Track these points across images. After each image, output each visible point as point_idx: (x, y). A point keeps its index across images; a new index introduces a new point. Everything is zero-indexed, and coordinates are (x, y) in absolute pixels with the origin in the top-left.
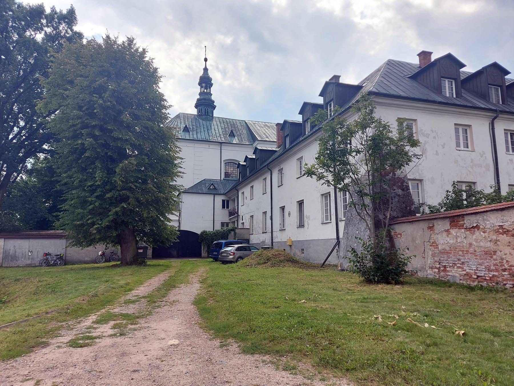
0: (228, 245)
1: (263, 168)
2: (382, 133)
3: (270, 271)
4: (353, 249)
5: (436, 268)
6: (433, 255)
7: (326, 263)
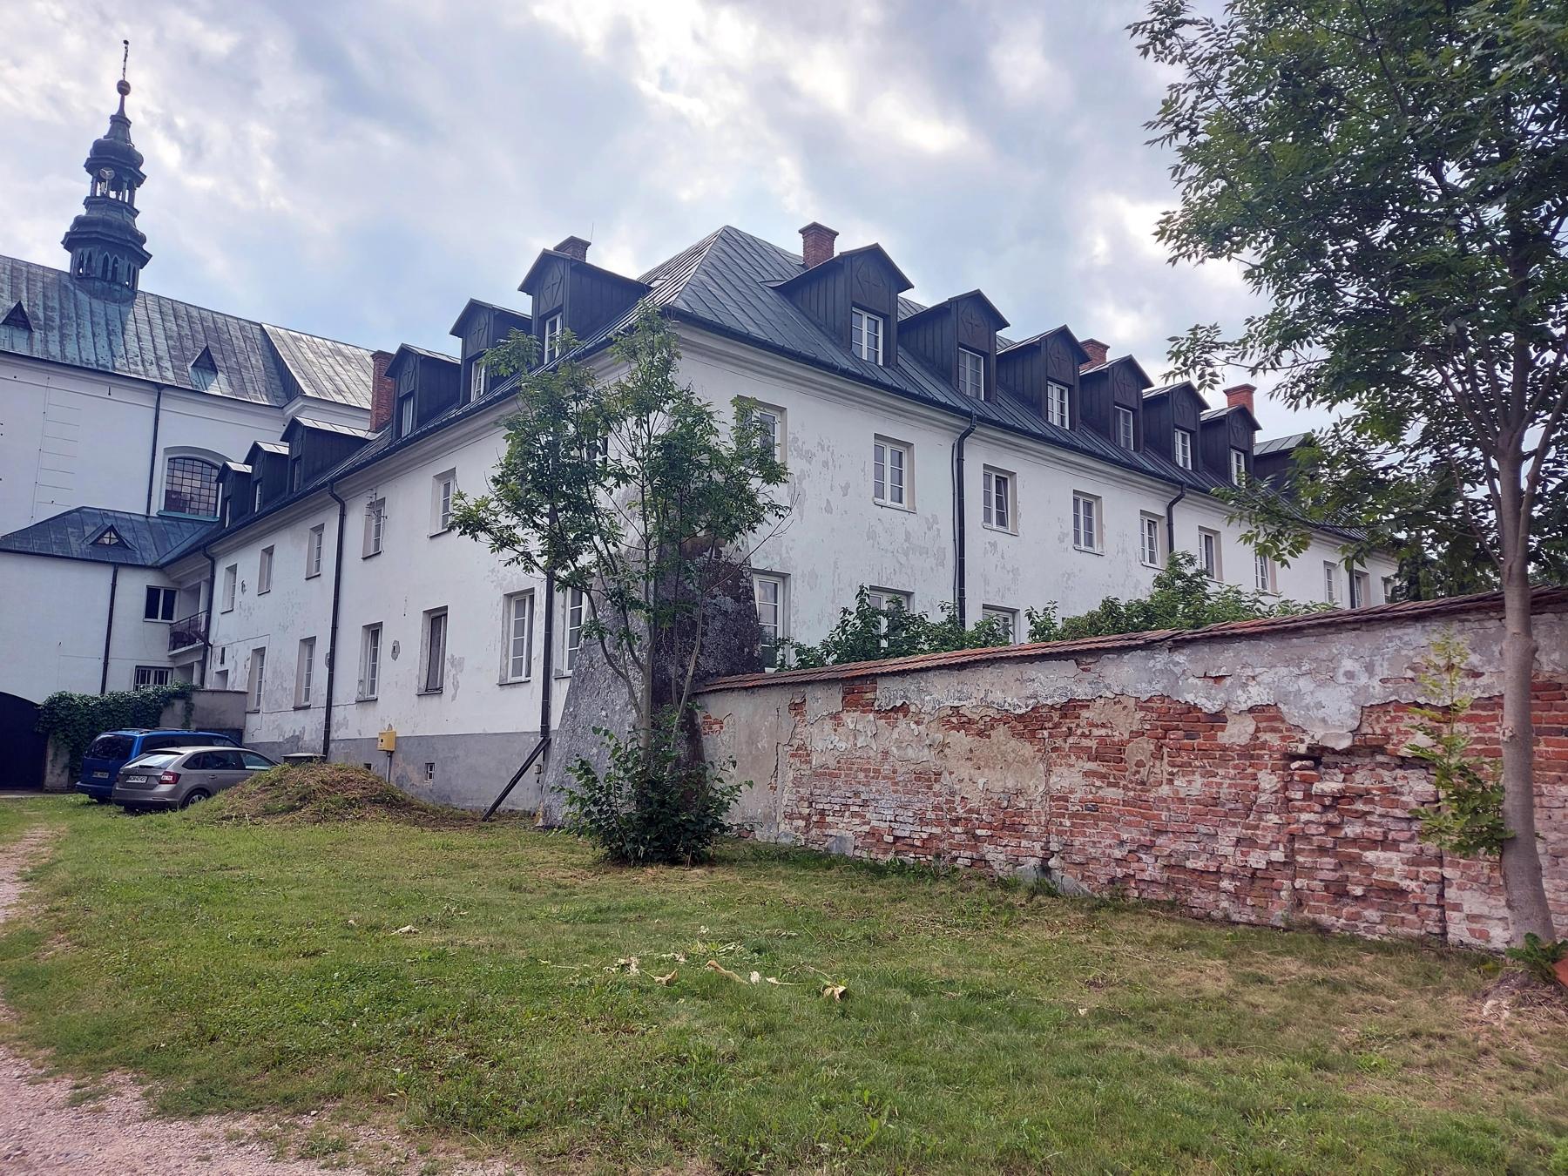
0: (151, 746)
1: (314, 490)
2: (691, 432)
3: (305, 834)
4: (583, 763)
5: (801, 817)
6: (797, 782)
7: (502, 806)
